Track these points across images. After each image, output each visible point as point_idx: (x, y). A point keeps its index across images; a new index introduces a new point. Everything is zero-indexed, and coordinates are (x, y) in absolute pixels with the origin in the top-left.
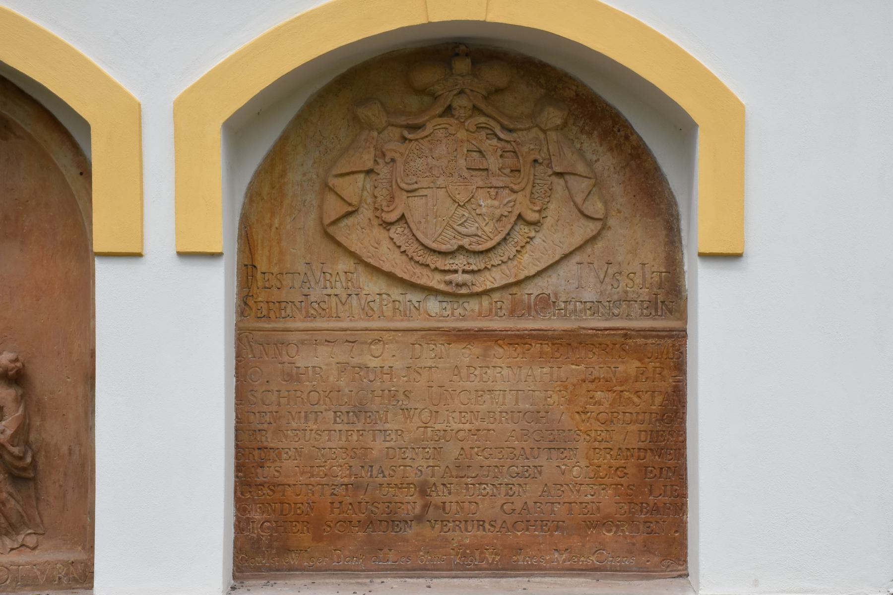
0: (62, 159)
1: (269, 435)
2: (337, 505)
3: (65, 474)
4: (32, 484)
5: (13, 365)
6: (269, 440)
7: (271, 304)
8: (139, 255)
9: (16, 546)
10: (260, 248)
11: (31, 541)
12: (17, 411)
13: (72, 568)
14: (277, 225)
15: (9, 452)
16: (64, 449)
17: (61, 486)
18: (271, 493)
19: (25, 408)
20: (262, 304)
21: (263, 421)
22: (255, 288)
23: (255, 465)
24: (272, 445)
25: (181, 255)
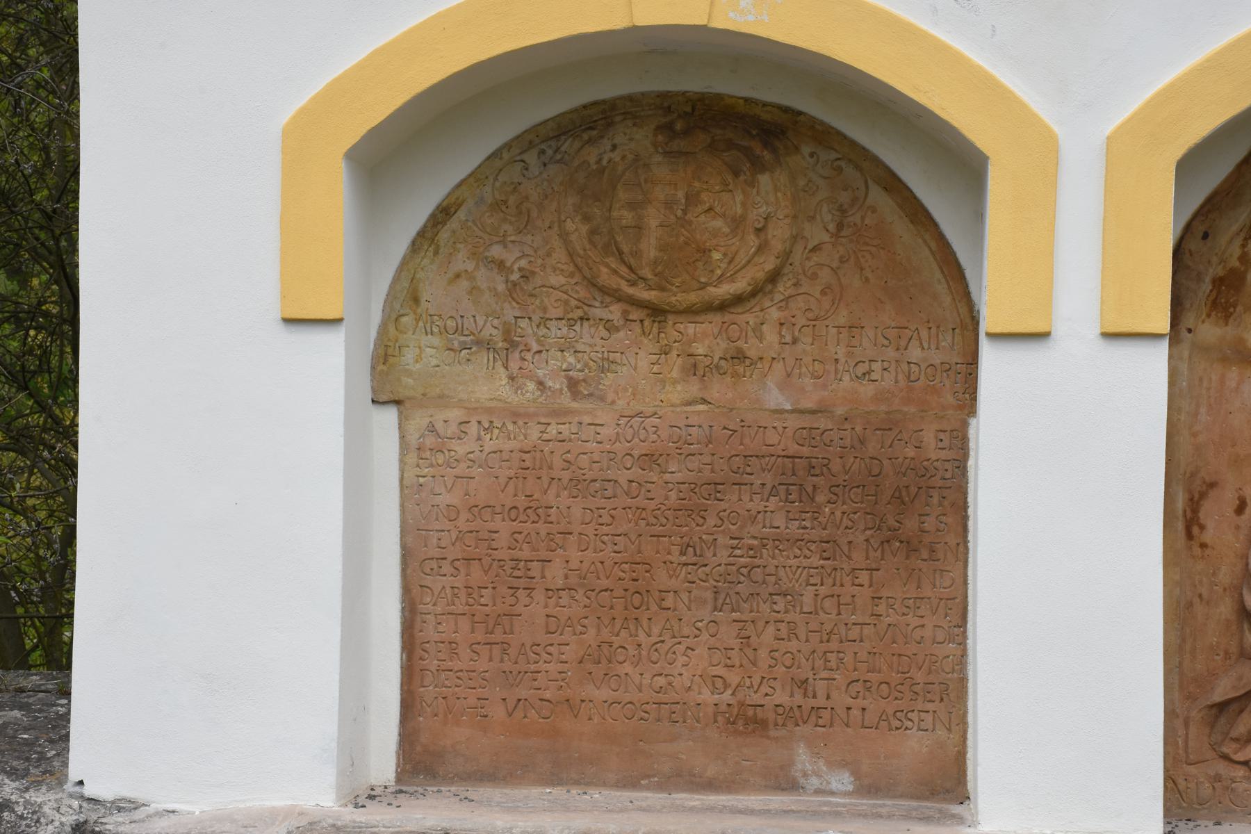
2: (855, 712)
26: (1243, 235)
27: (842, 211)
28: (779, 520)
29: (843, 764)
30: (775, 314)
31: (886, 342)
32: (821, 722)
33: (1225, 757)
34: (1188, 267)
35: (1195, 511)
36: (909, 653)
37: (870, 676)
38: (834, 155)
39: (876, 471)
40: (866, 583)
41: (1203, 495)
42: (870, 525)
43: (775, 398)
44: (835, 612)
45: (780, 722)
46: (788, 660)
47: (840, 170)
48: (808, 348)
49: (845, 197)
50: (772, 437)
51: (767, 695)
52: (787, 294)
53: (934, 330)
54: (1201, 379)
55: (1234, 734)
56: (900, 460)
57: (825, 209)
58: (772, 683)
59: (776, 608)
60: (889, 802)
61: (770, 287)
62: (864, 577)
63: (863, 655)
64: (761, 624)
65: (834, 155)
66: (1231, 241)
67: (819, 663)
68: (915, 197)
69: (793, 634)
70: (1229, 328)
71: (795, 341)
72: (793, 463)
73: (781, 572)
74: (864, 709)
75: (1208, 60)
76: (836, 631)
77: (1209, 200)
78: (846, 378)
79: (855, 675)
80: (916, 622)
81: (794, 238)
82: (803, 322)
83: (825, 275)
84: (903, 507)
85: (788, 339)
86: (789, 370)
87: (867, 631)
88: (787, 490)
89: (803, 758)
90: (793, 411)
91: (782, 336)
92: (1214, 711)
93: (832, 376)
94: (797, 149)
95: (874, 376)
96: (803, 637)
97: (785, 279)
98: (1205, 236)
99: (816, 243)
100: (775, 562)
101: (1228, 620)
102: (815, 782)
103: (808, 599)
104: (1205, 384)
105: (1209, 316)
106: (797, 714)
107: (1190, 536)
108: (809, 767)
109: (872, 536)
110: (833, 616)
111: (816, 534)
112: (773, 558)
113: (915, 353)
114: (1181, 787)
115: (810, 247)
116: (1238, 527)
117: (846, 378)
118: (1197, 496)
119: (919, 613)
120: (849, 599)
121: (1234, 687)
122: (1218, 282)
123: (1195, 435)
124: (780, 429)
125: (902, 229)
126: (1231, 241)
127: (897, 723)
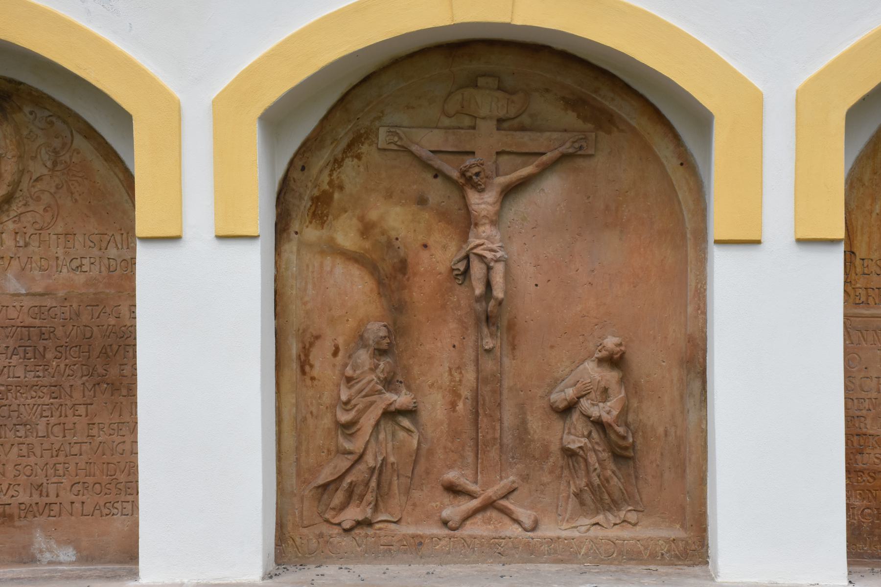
0: (665, 151)
1: (869, 421)
2: (77, 505)
3: (662, 454)
4: (631, 463)
5: (618, 349)
6: (868, 427)
7: (870, 291)
8: (758, 242)
9: (618, 522)
10: (859, 233)
11: (632, 517)
12: (620, 393)
13: (673, 545)
14: (878, 211)
15: (615, 431)
16: (661, 430)
17: (658, 466)
18: (871, 480)
19: (625, 388)
20: (860, 291)
21: (862, 407)
22: (854, 275)
23: (854, 451)
24: (871, 432)
25: (800, 241)
26: (329, 168)
27: (56, 152)
28: (20, 372)
29: (68, 542)
30: (11, 226)
31: (92, 245)
32: (52, 513)
33: (327, 521)
34: (293, 190)
35: (307, 355)
36: (115, 462)
37: (87, 479)
38: (47, 113)
39: (88, 335)
40: (84, 414)
41: (312, 344)
42: (85, 373)
43: (14, 285)
44: (61, 435)
45: (23, 515)
46: (28, 471)
47: (52, 123)
48: (36, 249)
49: (57, 143)
50: (13, 314)
51: (13, 496)
52: (19, 212)
53: (125, 235)
54: (308, 266)
55: (332, 506)
56: (105, 327)
57: (43, 151)
58: (16, 488)
59: (18, 434)
60: (100, 567)
61: (6, 207)
62: (82, 410)
63: (82, 465)
64: (8, 446)
65: (47, 113)
66: (321, 171)
67: (51, 472)
68: (107, 143)
69: (31, 451)
70: (324, 231)
71: (26, 245)
72: (29, 331)
73: (22, 409)
74: (83, 503)
75: (273, 50)
76: (62, 449)
77: (304, 144)
78: (65, 270)
79: (77, 479)
80: (118, 439)
81: (22, 172)
82: (32, 231)
83: (46, 198)
84: (94, 356)
85: (22, 243)
86: (23, 265)
87: (85, 447)
88: (25, 350)
89: (39, 540)
90: (27, 295)
91: (17, 242)
92: (320, 490)
93: (54, 269)
94: (20, 109)
95: (84, 268)
96: (38, 453)
97: (17, 201)
98: (303, 169)
99: (38, 175)
100: (18, 402)
101: (329, 428)
102: (48, 556)
103: (41, 428)
104: (311, 269)
105: (311, 222)
106: (35, 509)
107: (303, 372)
108: (44, 546)
109: (87, 381)
110: (60, 438)
111: (46, 381)
112: (16, 399)
113: (112, 252)
114: (297, 543)
115: (34, 178)
116: (334, 365)
117: (65, 270)
118: (307, 345)
119: (121, 433)
120: (71, 426)
121: (331, 474)
122: (315, 200)
123: (305, 304)
124: (18, 308)
125: (98, 165)
126: (321, 171)
127: (106, 511)
